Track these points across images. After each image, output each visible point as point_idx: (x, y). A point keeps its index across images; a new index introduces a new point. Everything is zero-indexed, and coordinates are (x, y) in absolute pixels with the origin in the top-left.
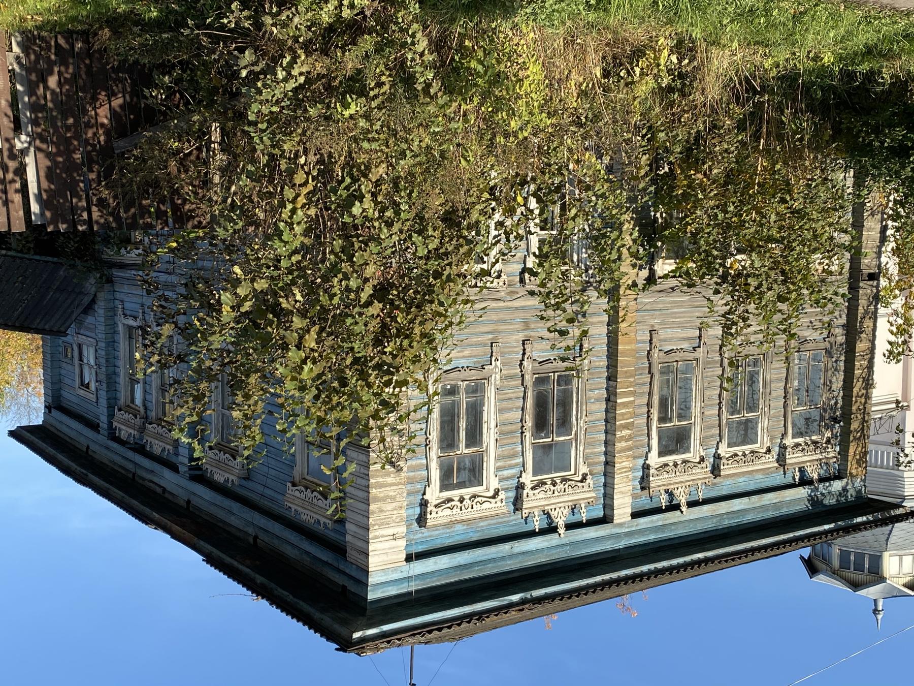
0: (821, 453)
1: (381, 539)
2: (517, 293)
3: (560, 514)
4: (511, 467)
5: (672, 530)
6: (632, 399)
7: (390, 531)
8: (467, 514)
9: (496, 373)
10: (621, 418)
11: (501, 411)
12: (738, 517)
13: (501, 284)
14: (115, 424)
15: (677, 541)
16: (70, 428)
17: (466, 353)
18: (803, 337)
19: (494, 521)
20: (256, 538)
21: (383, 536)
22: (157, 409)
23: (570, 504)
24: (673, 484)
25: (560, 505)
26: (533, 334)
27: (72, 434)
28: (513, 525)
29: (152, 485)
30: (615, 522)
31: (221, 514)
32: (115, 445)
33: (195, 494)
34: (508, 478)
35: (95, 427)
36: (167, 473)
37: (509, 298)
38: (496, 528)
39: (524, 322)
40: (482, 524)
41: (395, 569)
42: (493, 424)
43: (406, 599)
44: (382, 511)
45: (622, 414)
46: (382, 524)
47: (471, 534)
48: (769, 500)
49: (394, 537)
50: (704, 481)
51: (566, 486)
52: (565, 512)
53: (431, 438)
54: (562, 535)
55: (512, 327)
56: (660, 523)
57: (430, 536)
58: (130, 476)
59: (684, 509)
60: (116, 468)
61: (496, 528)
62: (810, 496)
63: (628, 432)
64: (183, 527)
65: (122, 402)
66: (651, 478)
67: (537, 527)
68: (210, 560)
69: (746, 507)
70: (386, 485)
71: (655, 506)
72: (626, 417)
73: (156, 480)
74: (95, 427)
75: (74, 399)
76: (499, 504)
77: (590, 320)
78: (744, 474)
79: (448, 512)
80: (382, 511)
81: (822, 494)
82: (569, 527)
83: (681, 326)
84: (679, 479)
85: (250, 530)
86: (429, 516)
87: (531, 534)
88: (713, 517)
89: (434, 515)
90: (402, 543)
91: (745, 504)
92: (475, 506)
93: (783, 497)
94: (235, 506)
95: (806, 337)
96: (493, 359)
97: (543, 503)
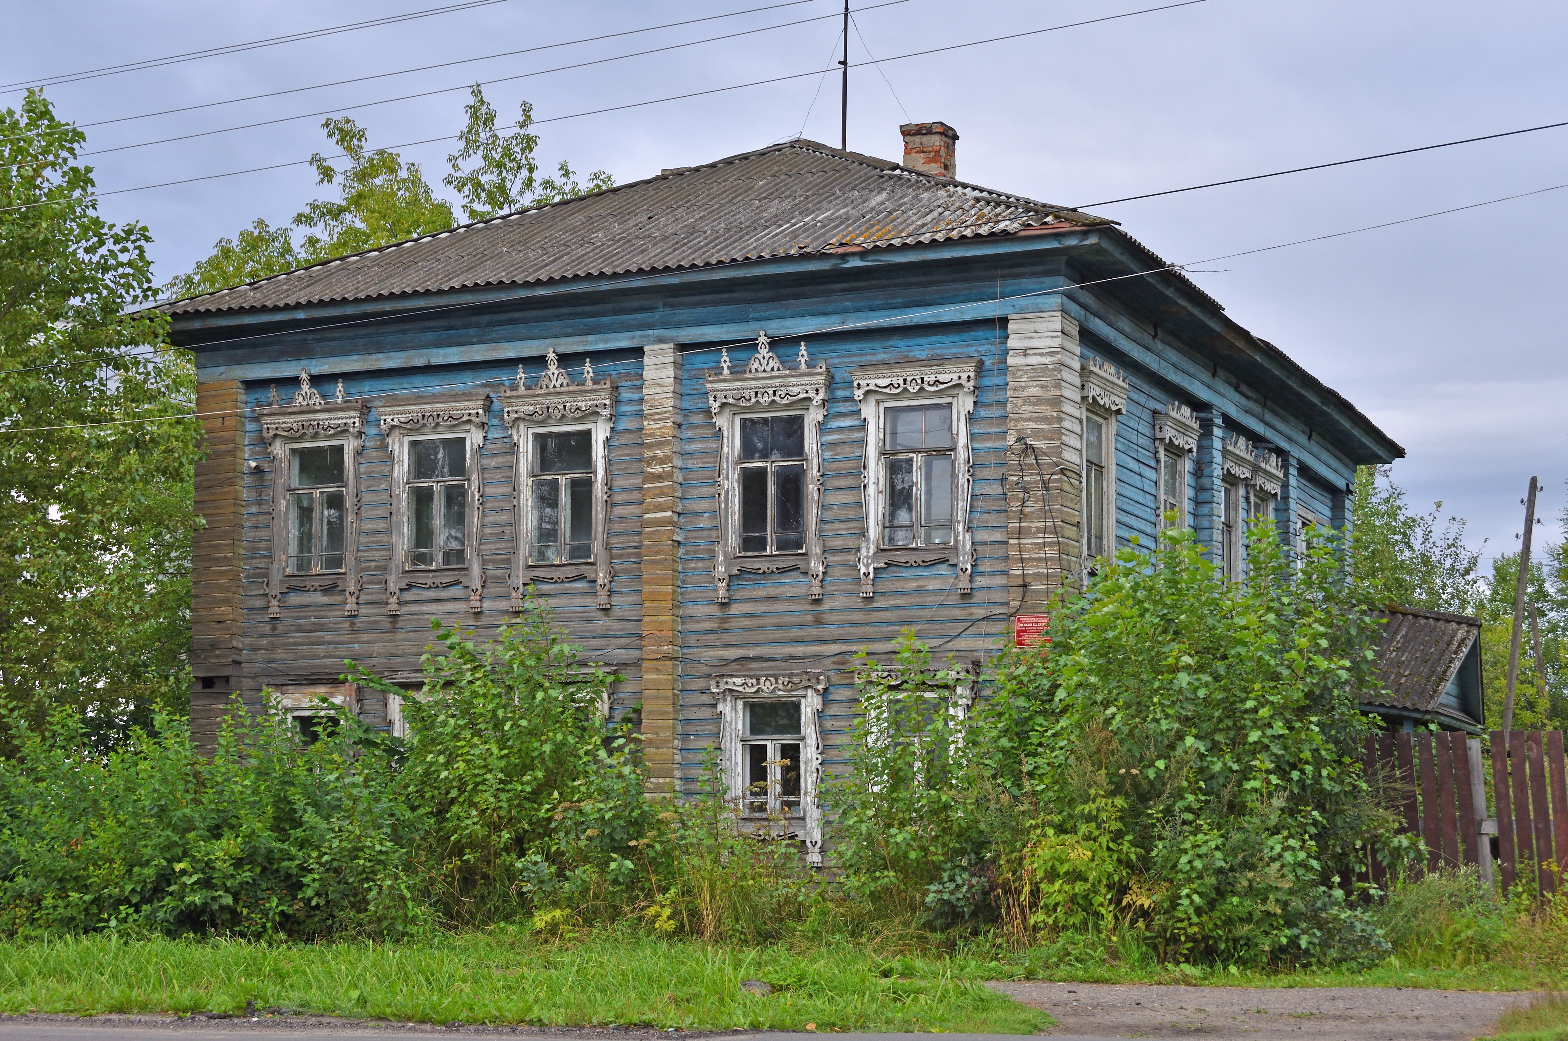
4: (841, 429)
6: (646, 516)
7: (1031, 360)
9: (867, 557)
11: (859, 505)
14: (1281, 475)
16: (1327, 467)
19: (864, 358)
20: (1154, 337)
21: (1042, 354)
22: (1237, 500)
23: (748, 375)
24: (569, 392)
26: (809, 608)
27: (1325, 456)
29: (1250, 394)
30: (671, 346)
31: (1186, 364)
32: (1283, 444)
33: (1208, 386)
34: (844, 415)
35: (1304, 471)
36: (1233, 412)
40: (886, 356)
41: (1023, 310)
42: (871, 489)
43: (1008, 271)
44: (1042, 387)
48: (391, 358)
49: (1025, 352)
50: (515, 393)
51: (753, 400)
52: (756, 365)
53: (967, 476)
54: (762, 333)
56: (591, 338)
58: (1269, 403)
59: (551, 356)
60: (1282, 412)
64: (1232, 346)
65: (1271, 506)
66: (607, 402)
68: (1214, 309)
69: (435, 351)
71: (606, 365)
73: (1244, 401)
74: (1304, 471)
75: (1318, 506)
76: (863, 383)
79: (941, 378)
84: (560, 399)
85: (1160, 346)
86: (972, 375)
87: (810, 338)
88: (497, 341)
89: (964, 376)
92: (901, 382)
94: (1174, 377)
96: (871, 576)
97: (794, 381)
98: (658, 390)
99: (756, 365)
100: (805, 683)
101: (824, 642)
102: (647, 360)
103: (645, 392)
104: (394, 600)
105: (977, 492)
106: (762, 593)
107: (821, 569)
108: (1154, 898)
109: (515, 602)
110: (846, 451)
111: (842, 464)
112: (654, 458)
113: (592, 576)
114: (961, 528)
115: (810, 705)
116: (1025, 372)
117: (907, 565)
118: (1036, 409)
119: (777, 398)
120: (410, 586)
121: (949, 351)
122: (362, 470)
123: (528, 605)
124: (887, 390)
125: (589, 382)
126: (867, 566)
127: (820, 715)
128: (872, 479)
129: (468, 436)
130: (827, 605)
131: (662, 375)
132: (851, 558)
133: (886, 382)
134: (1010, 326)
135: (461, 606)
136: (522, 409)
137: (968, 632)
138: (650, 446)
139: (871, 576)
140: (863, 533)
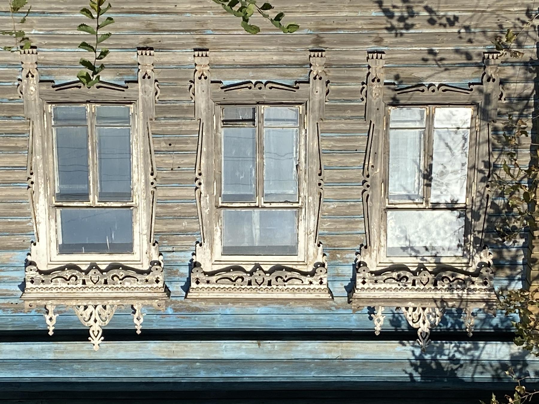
0: (450, 289)
3: (95, 316)
5: (74, 370)
12: (232, 370)
15: (84, 389)
18: (410, 79)
24: (77, 299)
48: (310, 352)
56: (51, 356)
62: (420, 358)
67: (51, 329)
78: (265, 302)
81: (452, 360)
84: (88, 293)
87: (368, 335)
91: (248, 351)
93: (348, 352)
95: (420, 79)
99: (105, 313)
104: (317, 70)
109: (147, 61)
113: (44, 87)
120: (294, 87)
122: (362, 226)
123: (133, 57)
125: (50, 308)
129: (217, 256)
135: (226, 58)
136: (139, 285)
140: (149, 120)
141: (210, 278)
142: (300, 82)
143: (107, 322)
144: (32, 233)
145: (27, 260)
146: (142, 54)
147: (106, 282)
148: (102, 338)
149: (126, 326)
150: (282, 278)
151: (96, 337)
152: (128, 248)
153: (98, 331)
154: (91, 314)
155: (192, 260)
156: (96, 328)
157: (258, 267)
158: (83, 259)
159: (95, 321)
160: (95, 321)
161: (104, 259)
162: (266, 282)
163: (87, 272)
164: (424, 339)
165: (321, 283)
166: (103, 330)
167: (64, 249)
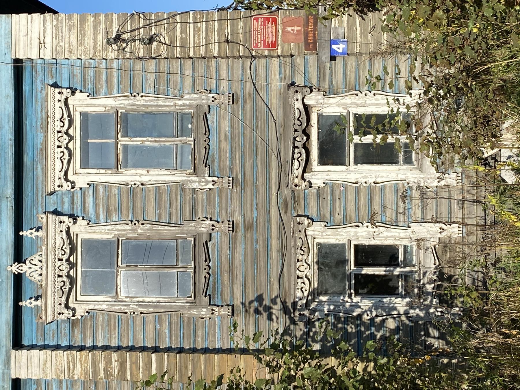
1: (42, 28)
2: (286, 213)
4: (96, 206)
8: (52, 138)
10: (134, 359)
13: (296, 181)
17: (224, 144)
21: (45, 30)
23: (44, 283)
25: (44, 268)
26: (239, 234)
28: (32, 208)
37: (281, 201)
38: (32, 188)
39: (253, 223)
42: (145, 179)
44: (70, 29)
45: (137, 363)
46: (57, 29)
47: (30, 154)
49: (42, 44)
51: (65, 279)
55: (249, 206)
57: (36, 100)
61: (32, 188)
63: (115, 372)
70: (95, 34)
72: (134, 366)
76: (58, 182)
77: (251, 320)
79: (58, 116)
80: (70, 29)
82: (18, 279)
83: (243, 69)
89: (58, 97)
90: (34, 55)
92: (59, 150)
96: (215, 179)
98: (49, 365)
99: (36, 275)
100: (302, 235)
101: (269, 221)
102: (22, 377)
103: (49, 378)
105: (152, 91)
106: (226, 277)
107: (208, 222)
108: (369, 332)
110: (114, 201)
111: (124, 205)
112: (106, 370)
114: (180, 102)
115: (320, 235)
116: (58, 43)
117: (207, 148)
118: (87, 34)
119: (65, 258)
121: (40, 114)
124: (65, 162)
126: (207, 182)
127: (331, 225)
128: (138, 178)
130: (238, 219)
131: (37, 361)
132: (200, 197)
133: (58, 163)
134: (21, 58)
137: (265, 98)
138: (95, 374)
139: (215, 179)
140: (181, 187)
141: (64, 233)
142: (209, 168)
143: (30, 278)
144: (95, 95)
145: (76, 89)
146: (229, 183)
147: (60, 276)
148: (16, 273)
149: (25, 213)
150: (64, 285)
151: (18, 268)
152: (85, 165)
153: (22, 270)
154: (35, 265)
155: (79, 217)
156: (24, 268)
157: (71, 138)
158: (76, 131)
159: (30, 268)
160: (30, 268)
161: (76, 146)
162: (60, 144)
163: (67, 133)
164: (18, 268)
165: (60, 314)
166: (22, 273)
167: (84, 116)
